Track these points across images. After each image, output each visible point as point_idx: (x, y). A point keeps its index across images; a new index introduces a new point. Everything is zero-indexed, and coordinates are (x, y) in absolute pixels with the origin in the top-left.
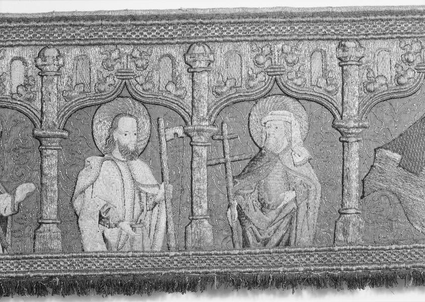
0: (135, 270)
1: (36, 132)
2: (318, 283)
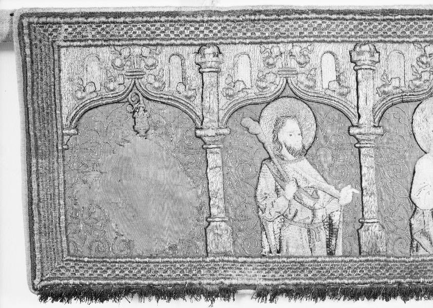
0: (182, 279)
2: (353, 294)
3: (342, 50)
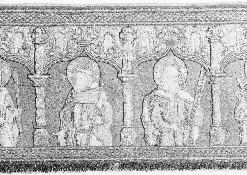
1: (118, 75)
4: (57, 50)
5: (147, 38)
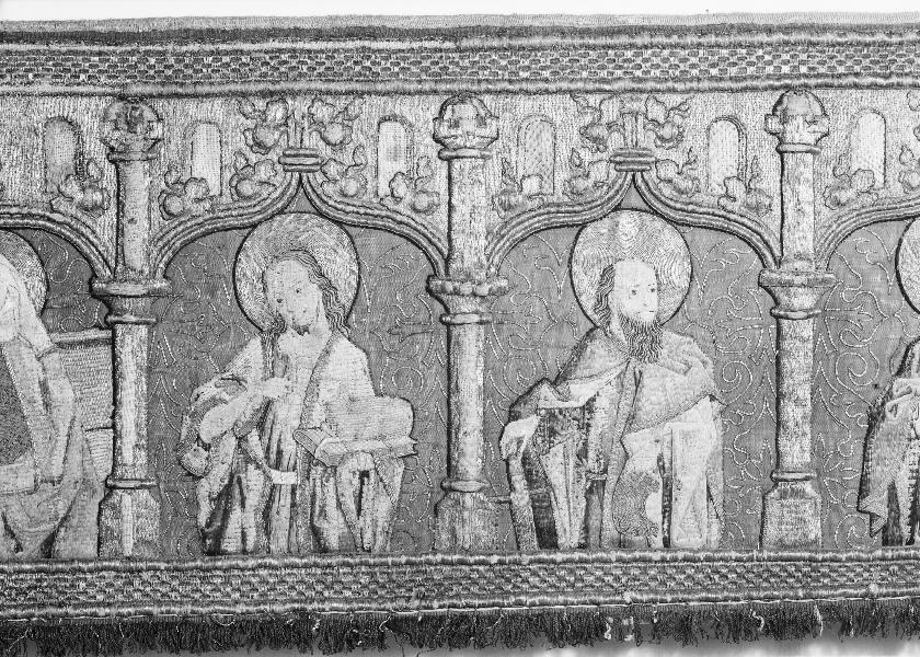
3: (422, 112)
4: (860, 183)
5: (542, 139)
